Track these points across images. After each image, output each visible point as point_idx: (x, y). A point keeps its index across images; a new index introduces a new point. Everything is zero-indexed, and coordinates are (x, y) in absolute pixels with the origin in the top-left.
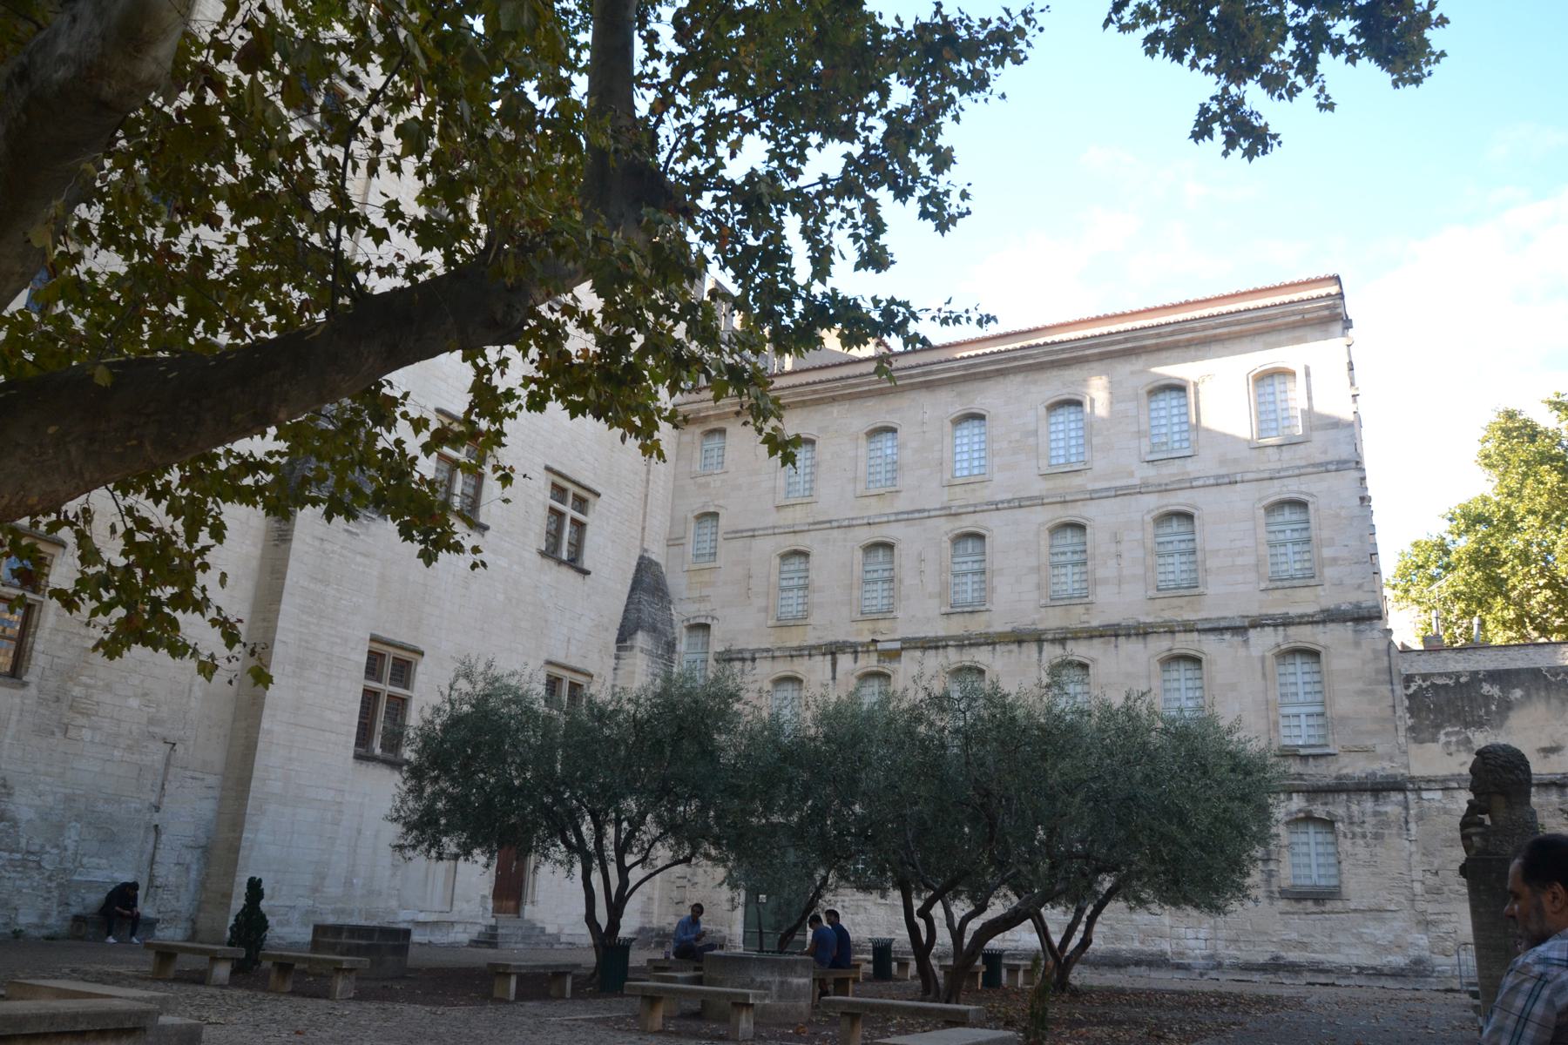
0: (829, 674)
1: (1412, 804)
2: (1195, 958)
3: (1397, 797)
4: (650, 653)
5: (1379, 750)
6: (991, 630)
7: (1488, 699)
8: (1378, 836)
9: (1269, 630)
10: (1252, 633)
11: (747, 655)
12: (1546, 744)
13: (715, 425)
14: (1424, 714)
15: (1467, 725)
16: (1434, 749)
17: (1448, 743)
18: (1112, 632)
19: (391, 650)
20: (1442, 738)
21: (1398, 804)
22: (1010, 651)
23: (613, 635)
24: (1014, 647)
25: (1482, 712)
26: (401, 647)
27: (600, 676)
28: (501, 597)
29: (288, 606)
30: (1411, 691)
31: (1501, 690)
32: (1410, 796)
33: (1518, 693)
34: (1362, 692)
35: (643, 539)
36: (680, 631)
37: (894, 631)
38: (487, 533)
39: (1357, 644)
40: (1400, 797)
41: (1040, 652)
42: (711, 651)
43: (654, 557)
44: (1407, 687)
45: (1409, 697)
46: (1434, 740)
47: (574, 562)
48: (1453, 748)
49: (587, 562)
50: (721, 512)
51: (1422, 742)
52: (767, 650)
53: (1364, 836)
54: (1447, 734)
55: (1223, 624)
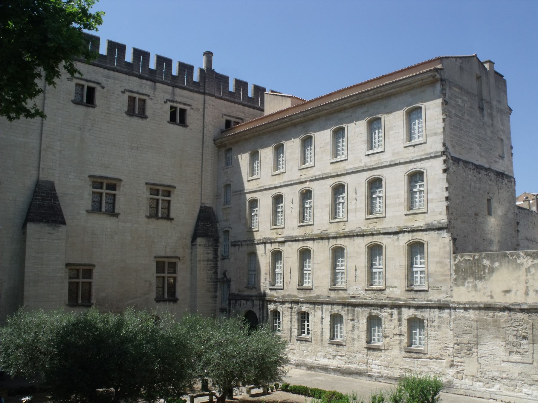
0: (264, 252)
1: (452, 314)
2: (375, 373)
3: (447, 311)
4: (205, 245)
5: (443, 289)
6: (313, 233)
7: (484, 267)
8: (439, 327)
9: (406, 234)
10: (401, 235)
11: (240, 243)
12: (505, 289)
13: (228, 147)
14: (460, 273)
15: (476, 279)
16: (462, 289)
17: (468, 287)
18: (351, 235)
19: (80, 267)
20: (466, 284)
21: (448, 313)
22: (319, 242)
23: (189, 241)
24: (321, 241)
25: (482, 273)
26: (85, 265)
27: (184, 257)
28: (129, 238)
29: (28, 264)
30: (456, 262)
31: (490, 262)
32: (452, 311)
33: (497, 264)
34: (438, 262)
35: (201, 199)
36: (221, 234)
37: (283, 233)
38: (120, 216)
39: (438, 240)
40: (448, 311)
41: (329, 243)
42: (230, 241)
43: (208, 205)
44: (455, 261)
45: (455, 265)
46: (463, 285)
47: (168, 217)
48: (470, 289)
49: (172, 215)
50: (232, 184)
51: (459, 286)
52: (245, 241)
53: (434, 327)
54: (468, 283)
55: (390, 231)
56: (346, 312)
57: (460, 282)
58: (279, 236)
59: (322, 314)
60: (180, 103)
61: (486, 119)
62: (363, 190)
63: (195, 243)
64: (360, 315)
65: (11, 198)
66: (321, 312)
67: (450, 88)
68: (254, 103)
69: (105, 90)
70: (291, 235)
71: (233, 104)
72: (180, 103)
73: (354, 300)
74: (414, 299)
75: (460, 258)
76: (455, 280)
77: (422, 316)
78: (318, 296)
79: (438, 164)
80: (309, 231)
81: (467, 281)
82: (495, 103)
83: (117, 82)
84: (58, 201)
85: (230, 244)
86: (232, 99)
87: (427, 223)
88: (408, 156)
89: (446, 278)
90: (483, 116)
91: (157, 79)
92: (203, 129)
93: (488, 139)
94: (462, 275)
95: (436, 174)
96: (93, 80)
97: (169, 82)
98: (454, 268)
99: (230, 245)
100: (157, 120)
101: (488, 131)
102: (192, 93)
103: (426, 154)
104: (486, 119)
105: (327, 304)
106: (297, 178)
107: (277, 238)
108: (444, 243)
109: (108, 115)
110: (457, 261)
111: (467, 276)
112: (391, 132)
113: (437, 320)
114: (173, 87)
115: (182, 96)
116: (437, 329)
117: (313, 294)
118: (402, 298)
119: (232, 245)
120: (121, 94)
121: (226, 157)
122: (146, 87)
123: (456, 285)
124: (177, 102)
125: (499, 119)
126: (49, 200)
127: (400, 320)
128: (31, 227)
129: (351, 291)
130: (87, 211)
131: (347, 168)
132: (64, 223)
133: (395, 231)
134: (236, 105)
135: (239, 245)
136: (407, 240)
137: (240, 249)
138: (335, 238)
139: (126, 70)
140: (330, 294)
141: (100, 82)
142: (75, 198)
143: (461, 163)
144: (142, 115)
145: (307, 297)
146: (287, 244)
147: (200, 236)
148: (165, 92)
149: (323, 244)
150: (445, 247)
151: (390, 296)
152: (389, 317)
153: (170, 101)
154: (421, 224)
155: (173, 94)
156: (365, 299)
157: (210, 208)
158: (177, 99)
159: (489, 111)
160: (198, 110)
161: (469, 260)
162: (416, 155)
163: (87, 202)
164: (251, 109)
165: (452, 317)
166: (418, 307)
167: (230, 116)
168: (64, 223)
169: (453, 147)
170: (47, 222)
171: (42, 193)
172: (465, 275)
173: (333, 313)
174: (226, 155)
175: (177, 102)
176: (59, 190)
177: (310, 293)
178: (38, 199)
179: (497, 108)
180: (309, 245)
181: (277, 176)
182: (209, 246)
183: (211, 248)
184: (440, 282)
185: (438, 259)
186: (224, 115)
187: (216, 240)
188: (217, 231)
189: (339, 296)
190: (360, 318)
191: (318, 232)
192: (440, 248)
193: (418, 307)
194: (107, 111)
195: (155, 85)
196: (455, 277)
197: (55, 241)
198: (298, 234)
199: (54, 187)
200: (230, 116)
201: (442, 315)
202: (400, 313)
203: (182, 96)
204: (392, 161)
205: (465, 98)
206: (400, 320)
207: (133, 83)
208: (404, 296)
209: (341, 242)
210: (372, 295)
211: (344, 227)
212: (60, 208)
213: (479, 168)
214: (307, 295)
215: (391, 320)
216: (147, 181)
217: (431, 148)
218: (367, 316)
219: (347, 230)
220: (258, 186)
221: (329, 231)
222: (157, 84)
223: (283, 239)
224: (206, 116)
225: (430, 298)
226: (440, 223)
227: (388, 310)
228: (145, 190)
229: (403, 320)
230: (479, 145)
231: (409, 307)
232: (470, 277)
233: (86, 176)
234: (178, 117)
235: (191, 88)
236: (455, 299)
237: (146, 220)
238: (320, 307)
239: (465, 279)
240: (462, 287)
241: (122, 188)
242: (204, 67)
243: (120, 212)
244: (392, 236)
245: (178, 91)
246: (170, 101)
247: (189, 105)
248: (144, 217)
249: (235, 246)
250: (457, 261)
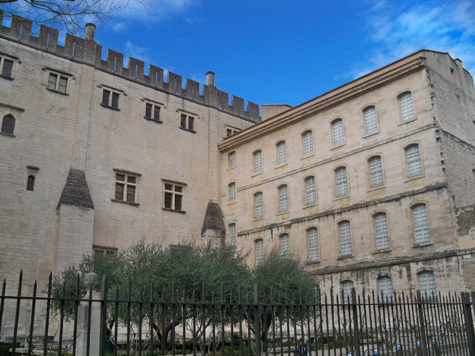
3: (454, 259)
6: (318, 212)
9: (408, 198)
10: (402, 200)
16: (467, 237)
18: (356, 207)
24: (326, 218)
28: (148, 226)
30: (458, 215)
32: (460, 258)
34: (441, 218)
36: (227, 227)
37: (289, 217)
38: (139, 207)
39: (438, 199)
41: (334, 218)
42: (236, 232)
43: (214, 202)
44: (456, 214)
45: (457, 217)
46: (467, 234)
50: (236, 182)
53: (444, 276)
54: (471, 231)
55: (392, 198)
56: (355, 277)
57: (464, 232)
58: (285, 221)
59: (332, 283)
60: (189, 113)
61: (462, 103)
62: (364, 166)
63: (204, 234)
64: (370, 278)
65: (47, 183)
66: (330, 282)
67: (433, 75)
68: (249, 117)
69: (127, 97)
70: (297, 217)
71: (232, 116)
72: (189, 113)
73: (362, 265)
74: (421, 254)
75: (461, 211)
76: (459, 230)
77: (431, 268)
78: (327, 268)
79: (431, 135)
80: (314, 211)
81: (470, 230)
82: (467, 93)
83: (137, 91)
84: (88, 188)
85: (236, 235)
86: (232, 112)
87: (426, 186)
88: (402, 133)
89: (450, 230)
90: (460, 102)
91: (170, 91)
92: (209, 135)
93: (466, 121)
94: (464, 225)
95: (430, 144)
96: (118, 88)
97: (180, 94)
98: (456, 220)
99: (236, 236)
100: (170, 126)
101: (465, 114)
102: (198, 105)
103: (419, 129)
104: (462, 103)
105: (336, 272)
106: (299, 168)
107: (283, 223)
108: (445, 201)
109: (130, 118)
110: (459, 213)
111: (470, 226)
112: (384, 116)
113: (446, 269)
114: (183, 98)
115: (191, 107)
116: (447, 278)
117: (321, 267)
118: (409, 255)
119: (238, 236)
120: (141, 101)
121: (229, 160)
122: (160, 97)
123: (461, 235)
124: (187, 112)
125: (472, 106)
126: (79, 186)
127: (409, 276)
128: (64, 208)
129: (359, 259)
130: (113, 201)
131: (346, 152)
132: (92, 207)
133: (397, 197)
134: (235, 118)
135: (245, 234)
136: (409, 203)
137: (247, 238)
138: (340, 213)
139: (144, 82)
140: (339, 264)
141: (123, 90)
142: (102, 188)
143: (449, 136)
144: (157, 120)
145: (316, 270)
146: (293, 226)
147: (209, 228)
148: (176, 103)
149: (329, 221)
150: (445, 204)
151: (398, 256)
152: (398, 275)
153: (180, 110)
154: (421, 188)
155: (183, 104)
156: (373, 262)
157: (216, 204)
158: (187, 109)
159: (464, 98)
160: (204, 119)
161: (470, 211)
162: (410, 130)
163: (111, 192)
164: (247, 122)
165: (460, 264)
166: (426, 260)
167: (230, 126)
168: (92, 207)
169: (441, 121)
170: (78, 205)
171: (75, 180)
172: (467, 225)
173: (343, 280)
174: (229, 158)
175: (187, 112)
176: (89, 179)
177: (318, 266)
178: (71, 185)
179: (469, 97)
180: (315, 223)
181: (280, 169)
182: (217, 237)
183: (219, 239)
184: (445, 234)
185: (440, 215)
186: (226, 125)
187: (224, 233)
188: (223, 224)
189: (348, 264)
190: (370, 281)
191: (323, 211)
192: (441, 206)
193: (426, 260)
194: (129, 115)
195: (168, 96)
196: (458, 228)
197: (85, 223)
198: (303, 216)
199: (84, 176)
200: (230, 126)
201: (450, 264)
202: (408, 269)
203: (191, 107)
204: (388, 139)
205: (445, 85)
206: (409, 276)
207: (151, 94)
208: (411, 254)
209: (345, 216)
210: (380, 258)
211: (348, 203)
212: (89, 194)
213: (463, 142)
214: (316, 269)
215: (401, 278)
216: (163, 178)
217: (423, 123)
218: (377, 277)
219: (351, 205)
220: (262, 180)
221: (334, 209)
222: (170, 95)
223: (290, 222)
224: (211, 125)
225: (436, 251)
226: (438, 184)
227: (397, 268)
228: (161, 185)
229: (412, 275)
230: (460, 124)
231: (417, 261)
232: (472, 225)
233: (111, 169)
234: (187, 123)
235: (198, 101)
236: (461, 247)
237: (162, 211)
238: (330, 276)
239: (468, 228)
240: (466, 236)
241: (141, 182)
242: (207, 83)
243: (139, 203)
244: (394, 203)
245: (187, 102)
246: (180, 110)
247: (197, 115)
248: (160, 208)
249: (242, 235)
250: (459, 213)
